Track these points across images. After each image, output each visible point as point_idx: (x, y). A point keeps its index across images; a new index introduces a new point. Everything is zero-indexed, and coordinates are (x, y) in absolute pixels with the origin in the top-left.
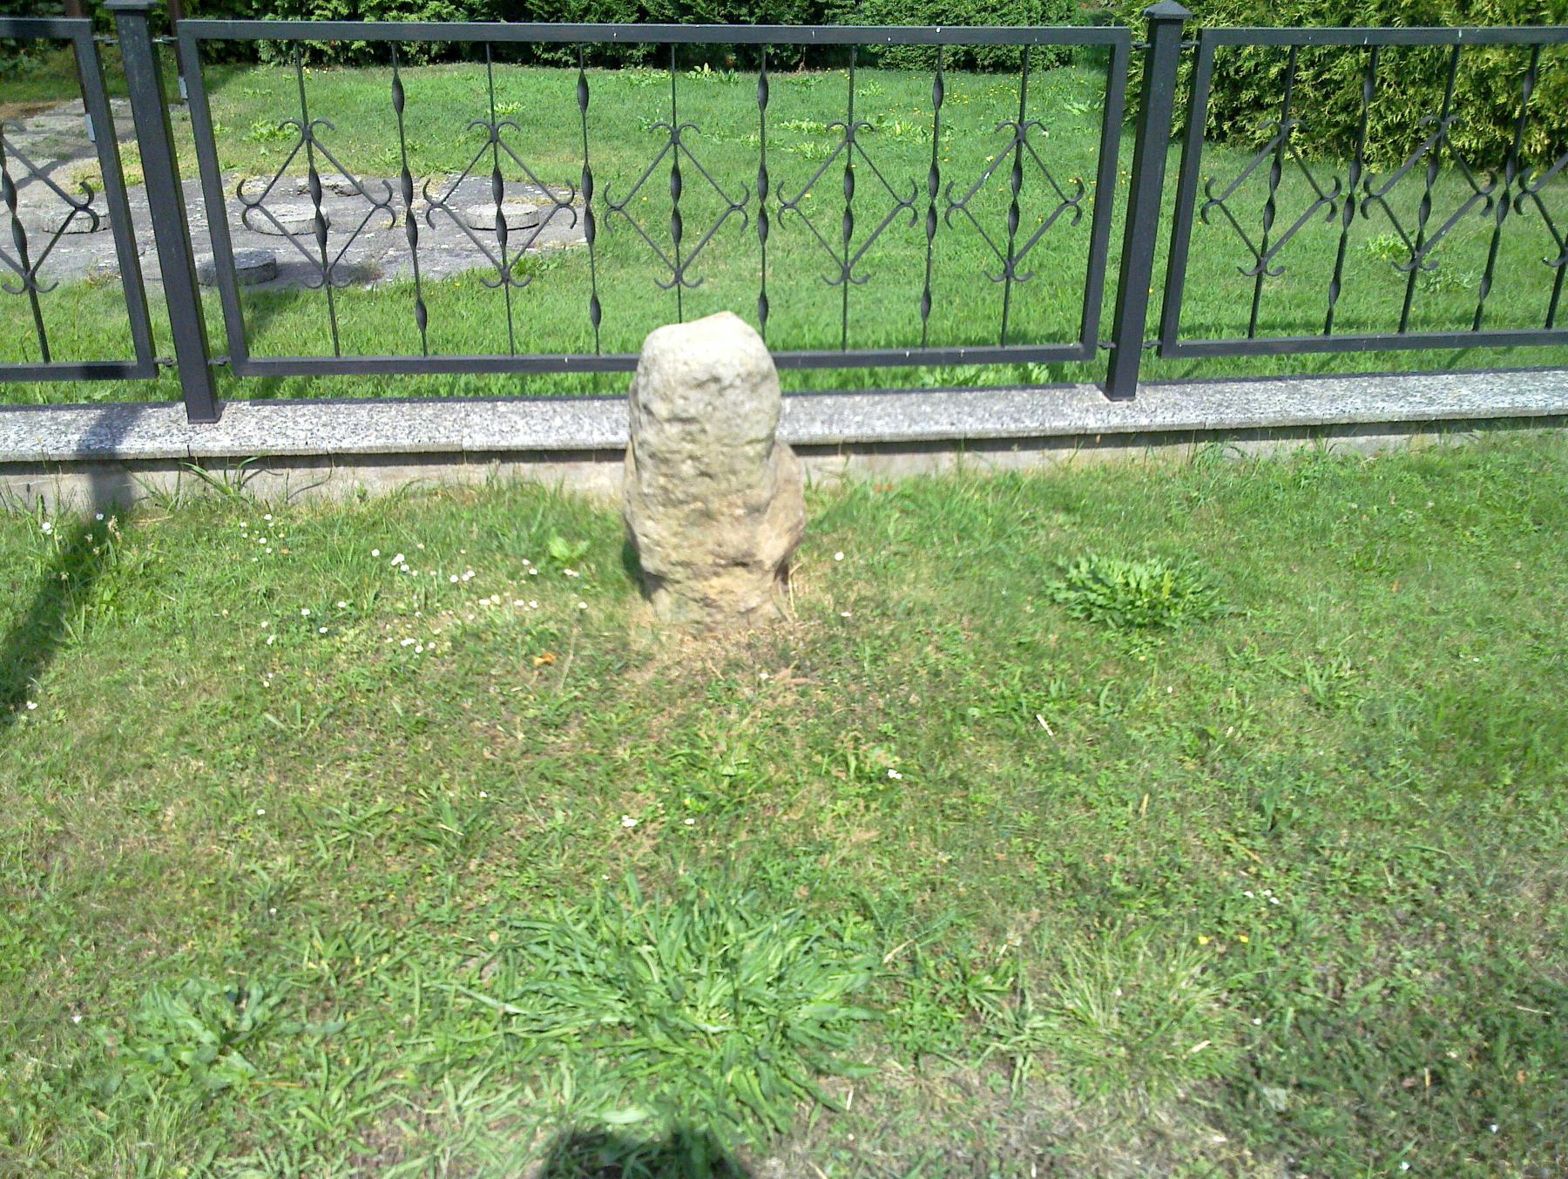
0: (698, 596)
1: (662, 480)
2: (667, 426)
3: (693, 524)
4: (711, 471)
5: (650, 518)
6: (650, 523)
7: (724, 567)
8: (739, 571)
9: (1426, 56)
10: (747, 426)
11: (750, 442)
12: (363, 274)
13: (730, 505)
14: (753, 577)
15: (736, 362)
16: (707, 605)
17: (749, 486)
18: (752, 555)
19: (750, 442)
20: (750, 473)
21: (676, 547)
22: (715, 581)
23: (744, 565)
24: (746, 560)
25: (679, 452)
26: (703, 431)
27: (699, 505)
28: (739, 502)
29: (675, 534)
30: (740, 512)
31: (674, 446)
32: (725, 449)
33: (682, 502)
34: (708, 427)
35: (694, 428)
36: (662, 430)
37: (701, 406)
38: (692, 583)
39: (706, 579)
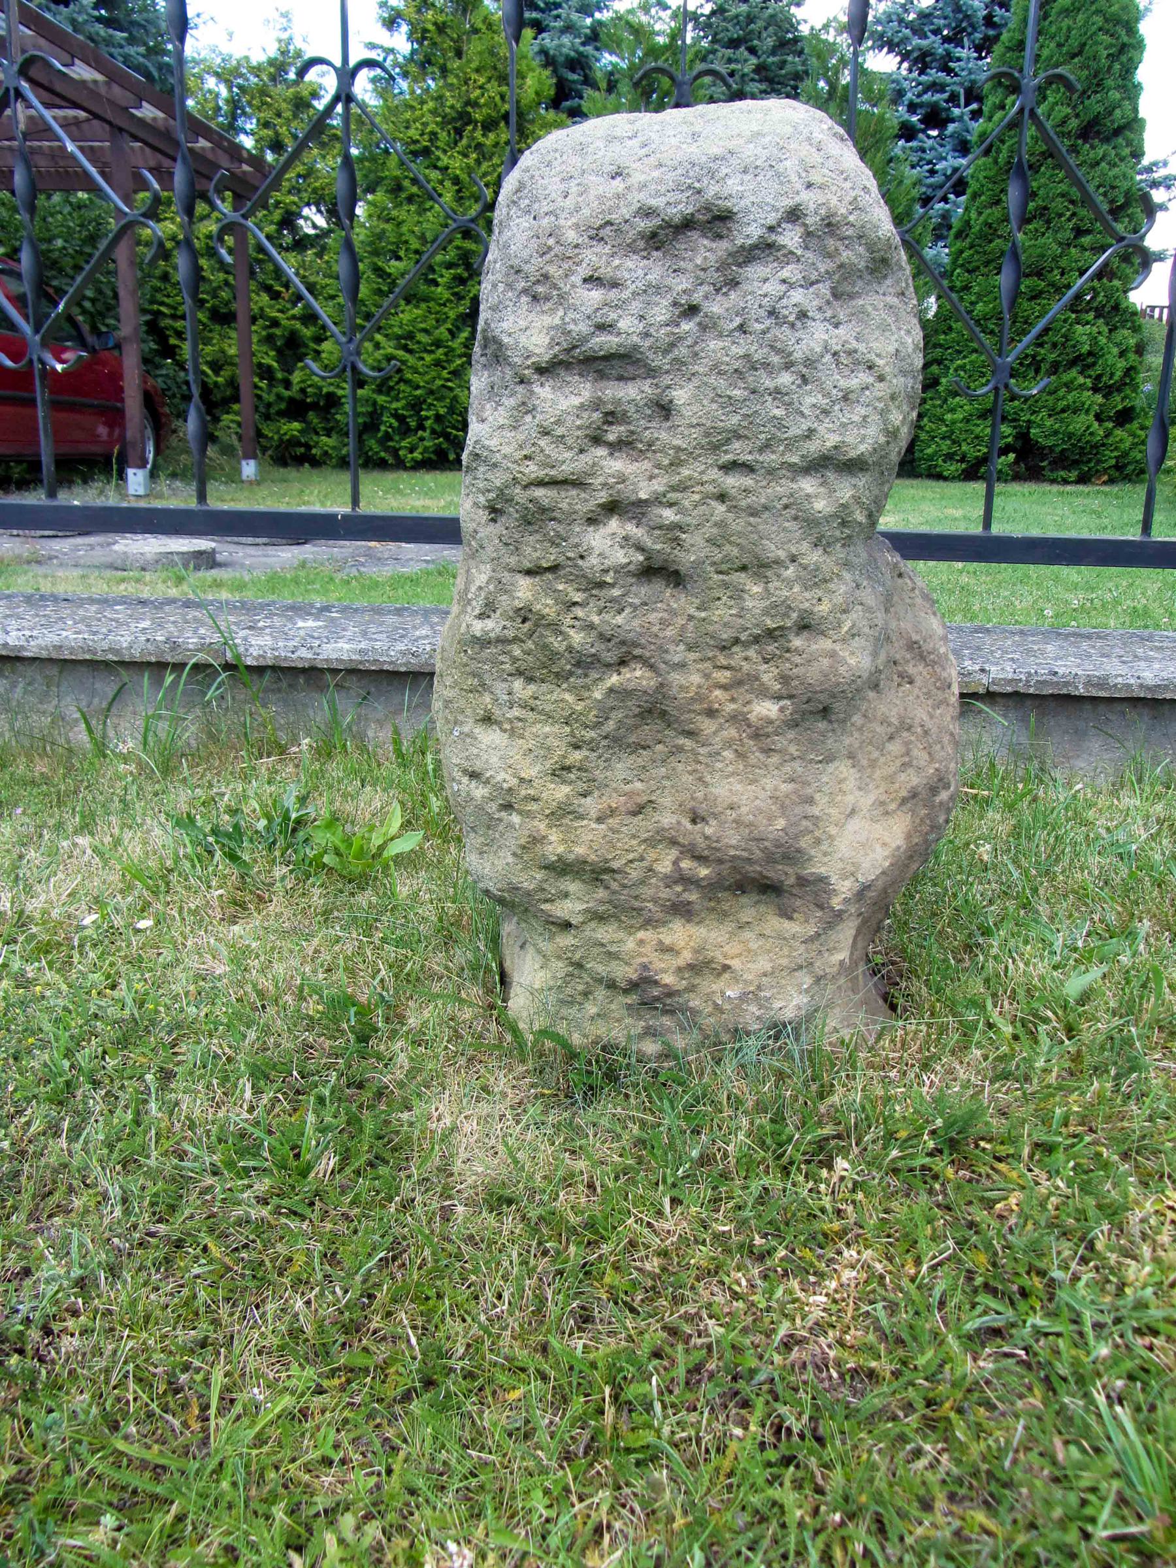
0: (624, 972)
1: (524, 589)
2: (544, 392)
3: (616, 741)
4: (686, 559)
5: (487, 720)
6: (491, 737)
7: (711, 889)
8: (748, 909)
9: (1112, 1004)
10: (811, 399)
11: (821, 464)
12: (664, 1328)
13: (741, 682)
14: (792, 928)
15: (790, 165)
16: (648, 1004)
17: (805, 626)
18: (790, 855)
19: (821, 464)
20: (816, 580)
21: (562, 813)
22: (678, 933)
23: (768, 889)
24: (774, 873)
25: (577, 483)
26: (664, 409)
27: (636, 676)
28: (769, 676)
29: (561, 771)
30: (767, 709)
31: (569, 463)
32: (732, 482)
33: (584, 663)
34: (681, 396)
35: (631, 393)
36: (526, 408)
37: (661, 312)
38: (605, 933)
39: (649, 923)
